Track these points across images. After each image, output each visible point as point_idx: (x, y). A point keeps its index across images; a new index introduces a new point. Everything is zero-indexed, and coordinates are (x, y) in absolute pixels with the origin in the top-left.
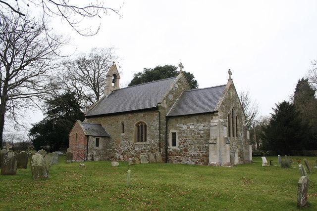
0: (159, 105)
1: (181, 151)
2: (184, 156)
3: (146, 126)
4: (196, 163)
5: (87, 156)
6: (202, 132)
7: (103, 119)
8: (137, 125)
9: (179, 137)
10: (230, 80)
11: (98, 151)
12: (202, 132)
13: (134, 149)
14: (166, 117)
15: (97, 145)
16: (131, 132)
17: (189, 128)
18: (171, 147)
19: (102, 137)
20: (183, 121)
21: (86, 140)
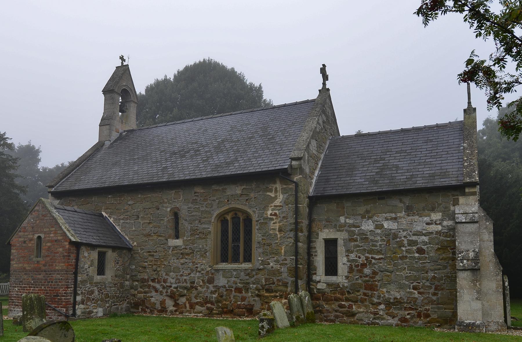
0: (294, 163)
1: (354, 288)
2: (362, 301)
3: (248, 220)
4: (403, 320)
5: (75, 303)
6: (426, 239)
7: (110, 200)
8: (222, 219)
9: (349, 251)
10: (325, 92)
11: (101, 286)
12: (426, 239)
13: (211, 281)
14: (310, 198)
15: (101, 271)
16: (205, 235)
17: (380, 226)
18: (320, 275)
19: (114, 248)
20: (362, 209)
21: (73, 256)
